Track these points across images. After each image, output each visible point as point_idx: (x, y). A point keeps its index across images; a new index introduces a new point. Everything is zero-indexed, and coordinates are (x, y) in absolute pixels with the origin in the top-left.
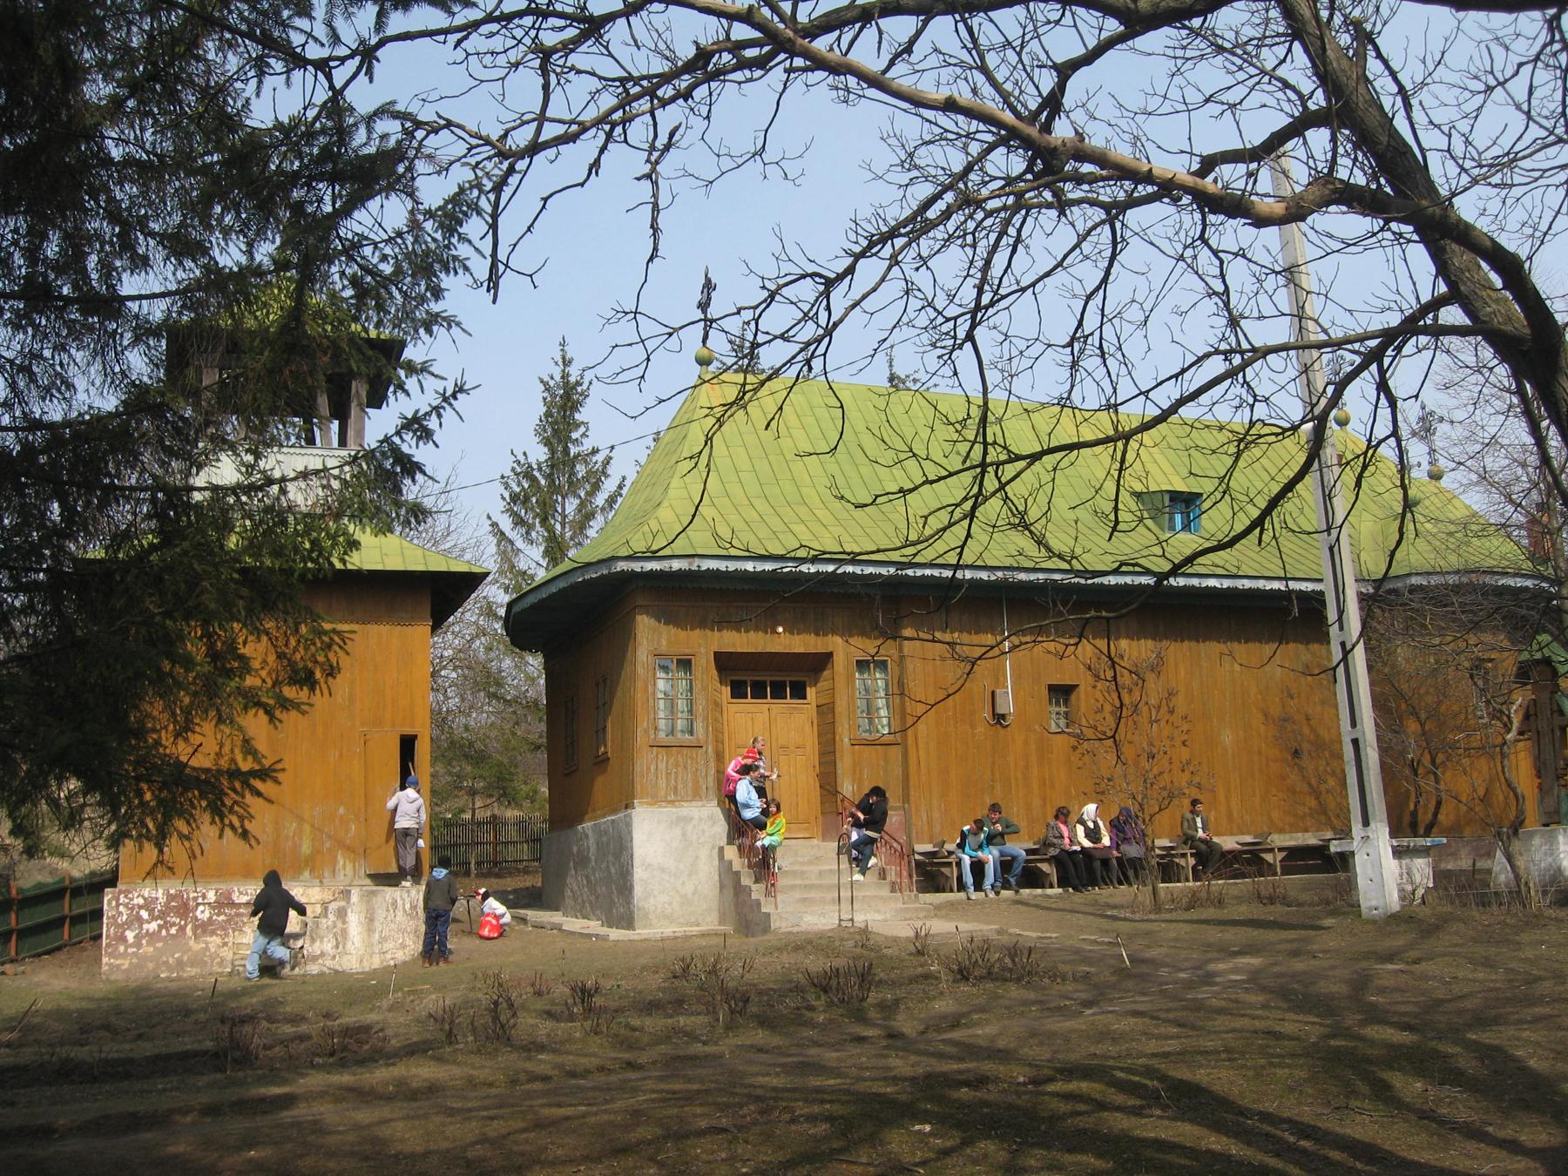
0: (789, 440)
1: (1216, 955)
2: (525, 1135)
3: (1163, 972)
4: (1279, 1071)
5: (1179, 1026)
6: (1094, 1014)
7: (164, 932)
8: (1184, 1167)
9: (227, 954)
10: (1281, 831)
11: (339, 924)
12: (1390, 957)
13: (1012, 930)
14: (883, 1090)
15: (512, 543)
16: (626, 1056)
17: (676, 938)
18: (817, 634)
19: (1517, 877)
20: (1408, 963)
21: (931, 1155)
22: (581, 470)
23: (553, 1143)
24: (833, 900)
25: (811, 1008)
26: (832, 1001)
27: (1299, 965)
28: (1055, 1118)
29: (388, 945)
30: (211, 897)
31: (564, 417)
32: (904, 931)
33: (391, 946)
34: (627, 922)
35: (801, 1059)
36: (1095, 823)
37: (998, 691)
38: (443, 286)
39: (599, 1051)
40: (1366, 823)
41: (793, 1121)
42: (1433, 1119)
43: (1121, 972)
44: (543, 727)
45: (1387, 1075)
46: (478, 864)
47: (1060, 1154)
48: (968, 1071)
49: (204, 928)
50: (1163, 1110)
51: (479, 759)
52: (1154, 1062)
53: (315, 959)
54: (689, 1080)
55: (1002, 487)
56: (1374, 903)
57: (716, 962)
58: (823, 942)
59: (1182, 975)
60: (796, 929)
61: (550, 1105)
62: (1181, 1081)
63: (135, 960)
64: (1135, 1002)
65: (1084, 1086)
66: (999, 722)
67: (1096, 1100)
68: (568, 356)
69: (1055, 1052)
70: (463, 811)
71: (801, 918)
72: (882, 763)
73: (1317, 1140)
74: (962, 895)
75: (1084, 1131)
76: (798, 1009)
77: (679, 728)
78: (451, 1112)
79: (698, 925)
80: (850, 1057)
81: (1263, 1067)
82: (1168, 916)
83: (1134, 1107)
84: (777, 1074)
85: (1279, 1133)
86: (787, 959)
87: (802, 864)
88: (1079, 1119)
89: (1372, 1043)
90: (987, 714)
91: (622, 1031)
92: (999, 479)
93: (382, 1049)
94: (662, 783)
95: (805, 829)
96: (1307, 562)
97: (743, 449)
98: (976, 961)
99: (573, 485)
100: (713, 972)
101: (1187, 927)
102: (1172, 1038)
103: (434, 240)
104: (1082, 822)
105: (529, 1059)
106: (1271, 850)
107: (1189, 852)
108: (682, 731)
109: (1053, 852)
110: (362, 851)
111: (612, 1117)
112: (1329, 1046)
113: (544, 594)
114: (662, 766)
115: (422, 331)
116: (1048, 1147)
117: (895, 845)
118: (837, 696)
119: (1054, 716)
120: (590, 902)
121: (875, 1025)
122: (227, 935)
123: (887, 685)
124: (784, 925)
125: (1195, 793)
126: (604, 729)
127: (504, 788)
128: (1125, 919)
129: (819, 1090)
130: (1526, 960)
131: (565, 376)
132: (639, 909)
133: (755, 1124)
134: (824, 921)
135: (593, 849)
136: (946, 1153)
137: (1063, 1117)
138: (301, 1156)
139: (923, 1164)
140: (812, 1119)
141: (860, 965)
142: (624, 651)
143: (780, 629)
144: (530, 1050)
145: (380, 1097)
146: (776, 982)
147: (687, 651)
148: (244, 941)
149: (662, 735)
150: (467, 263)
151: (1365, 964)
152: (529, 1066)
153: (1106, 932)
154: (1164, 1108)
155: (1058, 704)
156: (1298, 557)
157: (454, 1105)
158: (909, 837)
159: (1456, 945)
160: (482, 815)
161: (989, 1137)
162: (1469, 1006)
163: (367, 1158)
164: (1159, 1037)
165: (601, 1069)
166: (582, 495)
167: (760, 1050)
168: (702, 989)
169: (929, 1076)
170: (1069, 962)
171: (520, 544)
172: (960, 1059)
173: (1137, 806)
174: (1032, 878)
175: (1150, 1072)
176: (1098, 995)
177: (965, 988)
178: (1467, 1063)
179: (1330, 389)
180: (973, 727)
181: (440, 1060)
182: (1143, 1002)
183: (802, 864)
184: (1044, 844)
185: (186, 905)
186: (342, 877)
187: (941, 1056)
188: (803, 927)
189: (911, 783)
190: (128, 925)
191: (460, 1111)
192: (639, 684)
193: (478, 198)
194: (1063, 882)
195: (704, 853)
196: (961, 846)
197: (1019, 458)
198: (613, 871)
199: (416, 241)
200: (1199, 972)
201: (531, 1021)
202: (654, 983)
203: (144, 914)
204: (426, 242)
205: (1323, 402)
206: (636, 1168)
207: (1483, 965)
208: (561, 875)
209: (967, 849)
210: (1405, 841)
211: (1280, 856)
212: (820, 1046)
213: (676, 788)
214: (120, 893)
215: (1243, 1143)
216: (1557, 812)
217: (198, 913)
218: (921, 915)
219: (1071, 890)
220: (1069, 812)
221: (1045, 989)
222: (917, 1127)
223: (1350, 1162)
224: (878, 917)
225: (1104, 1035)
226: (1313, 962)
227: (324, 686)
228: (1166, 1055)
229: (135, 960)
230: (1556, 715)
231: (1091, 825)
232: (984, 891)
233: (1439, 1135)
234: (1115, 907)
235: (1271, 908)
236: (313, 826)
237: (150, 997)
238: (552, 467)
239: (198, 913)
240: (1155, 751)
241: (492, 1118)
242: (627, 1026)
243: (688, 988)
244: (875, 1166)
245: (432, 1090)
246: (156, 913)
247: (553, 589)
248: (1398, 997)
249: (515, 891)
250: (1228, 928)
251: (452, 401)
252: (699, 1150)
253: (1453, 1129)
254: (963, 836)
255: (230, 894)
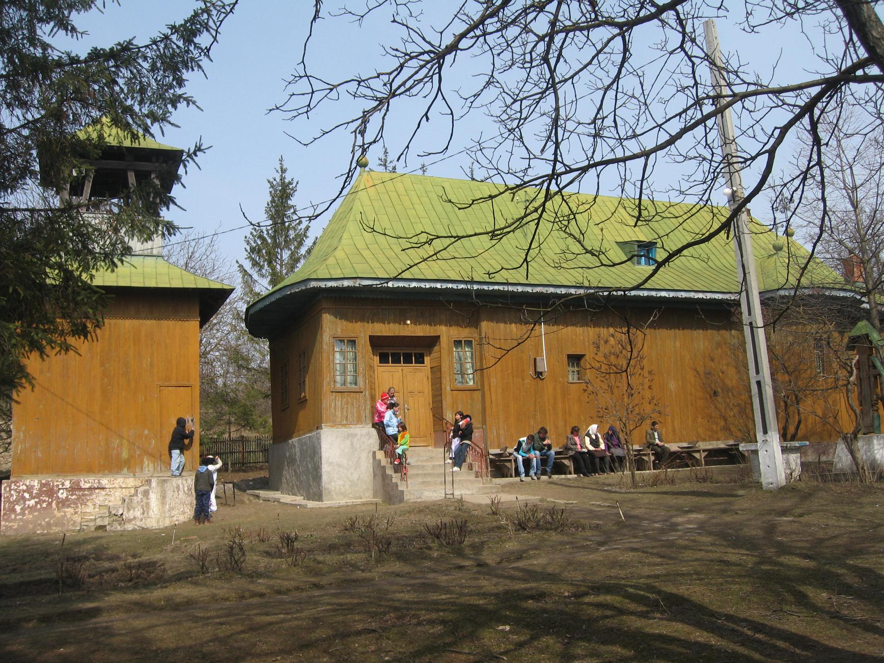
0: (413, 211)
1: (675, 513)
2: (243, 636)
3: (645, 523)
4: (735, 587)
5: (661, 557)
6: (606, 550)
7: (39, 506)
8: (681, 654)
9: (77, 518)
10: (704, 440)
11: (145, 500)
12: (784, 513)
13: (549, 499)
14: (477, 602)
15: (250, 276)
16: (314, 580)
17: (347, 506)
18: (431, 325)
19: (857, 464)
20: (795, 516)
21: (512, 647)
22: (292, 234)
23: (259, 641)
24: (441, 482)
25: (430, 548)
26: (442, 544)
27: (728, 518)
28: (591, 621)
29: (174, 513)
30: (68, 484)
31: (282, 202)
32: (485, 500)
33: (176, 513)
34: (319, 497)
35: (423, 581)
36: (596, 436)
37: (538, 358)
38: (184, 77)
39: (298, 577)
40: (765, 432)
41: (419, 624)
42: (840, 618)
43: (619, 523)
44: (269, 385)
45: (803, 589)
46: (233, 464)
47: (597, 645)
48: (532, 589)
49: (63, 503)
50: (661, 614)
51: (233, 403)
52: (649, 581)
53: (130, 521)
54: (351, 596)
55: (560, 190)
56: (770, 480)
57: (371, 520)
58: (436, 507)
59: (657, 525)
60: (419, 500)
61: (261, 614)
62: (671, 594)
63: (21, 523)
64: (631, 542)
65: (609, 598)
66: (538, 377)
67: (617, 608)
68: (284, 167)
69: (585, 575)
70: (223, 433)
71: (422, 493)
72: (470, 401)
73: (767, 634)
74: (518, 479)
75: (612, 629)
76: (421, 548)
77: (349, 381)
78: (196, 619)
79: (361, 498)
80: (454, 579)
81: (722, 584)
82: (641, 490)
83: (642, 612)
84: (408, 592)
85: (740, 628)
86: (414, 518)
87: (423, 461)
88: (607, 620)
89: (789, 567)
90: (532, 372)
91: (312, 564)
92: (558, 186)
93: (162, 577)
94: (339, 414)
95: (424, 441)
96: (718, 282)
97: (385, 216)
98: (529, 518)
99: (287, 243)
100: (369, 526)
101: (654, 496)
102: (658, 565)
103: (178, 47)
104: (588, 435)
105: (252, 582)
106: (699, 451)
107: (651, 452)
108: (351, 383)
109: (571, 453)
110: (159, 455)
111: (300, 622)
112: (761, 569)
113: (267, 302)
114: (339, 404)
115: (169, 106)
116: (589, 641)
117: (478, 449)
118: (442, 361)
119: (571, 373)
120: (297, 485)
121: (469, 559)
122: (77, 507)
123: (472, 355)
124: (412, 497)
125: (655, 416)
126: (304, 382)
127: (247, 420)
128: (616, 492)
129: (436, 603)
130: (868, 514)
131: (283, 179)
132: (325, 489)
133: (393, 626)
134: (436, 495)
135: (298, 454)
136: (521, 645)
137: (597, 620)
138: (93, 652)
139: (506, 653)
140: (431, 622)
141: (459, 520)
142: (315, 336)
143: (409, 322)
144: (252, 577)
145: (155, 608)
146: (407, 532)
147: (353, 335)
148: (88, 511)
149: (338, 385)
150: (200, 63)
151: (769, 518)
152: (252, 587)
153: (606, 500)
154: (663, 612)
155: (573, 366)
156: (712, 279)
157: (199, 615)
158: (486, 444)
159: (823, 505)
160: (234, 435)
161: (548, 634)
162: (841, 543)
163: (136, 653)
164: (649, 565)
165: (297, 589)
166: (293, 248)
167: (398, 575)
168: (361, 536)
169: (506, 593)
170: (586, 518)
171: (255, 276)
172: (525, 580)
173: (622, 425)
174: (559, 469)
175: (650, 588)
176: (607, 539)
177: (524, 535)
178: (851, 579)
179: (777, 132)
180: (523, 380)
181: (196, 584)
182: (635, 543)
183: (423, 461)
184: (566, 448)
185: (52, 489)
186: (147, 472)
187: (512, 578)
188: (424, 499)
189: (487, 414)
190: (17, 502)
191: (203, 618)
192: (325, 355)
193: (208, 19)
194: (577, 471)
195: (364, 455)
196: (517, 450)
197: (572, 171)
198: (310, 466)
199: (166, 47)
200: (667, 523)
201: (255, 558)
202: (334, 534)
203: (27, 495)
204: (173, 49)
205: (772, 141)
206: (315, 657)
207: (843, 517)
208: (280, 469)
209: (520, 452)
210: (789, 444)
211: (704, 454)
212: (435, 572)
213: (347, 417)
214: (12, 482)
215: (718, 636)
216: (872, 426)
217: (59, 494)
218: (494, 491)
219: (582, 475)
220: (579, 429)
221: (573, 534)
222: (501, 628)
223: (792, 648)
224: (468, 492)
225: (614, 564)
226: (736, 516)
227: (93, 334)
228: (657, 576)
229: (21, 523)
230: (871, 368)
231: (594, 437)
232: (531, 476)
233: (847, 629)
234: (609, 485)
235: (705, 484)
236: (129, 441)
237: (27, 546)
238: (275, 231)
239: (59, 494)
240: (632, 392)
241: (221, 624)
242: (315, 560)
243: (354, 536)
244: (474, 655)
245: (189, 603)
246: (34, 495)
247: (273, 299)
248: (794, 537)
249: (254, 480)
250: (679, 496)
251: (194, 157)
252: (357, 644)
253: (854, 625)
254: (520, 444)
255: (79, 482)
